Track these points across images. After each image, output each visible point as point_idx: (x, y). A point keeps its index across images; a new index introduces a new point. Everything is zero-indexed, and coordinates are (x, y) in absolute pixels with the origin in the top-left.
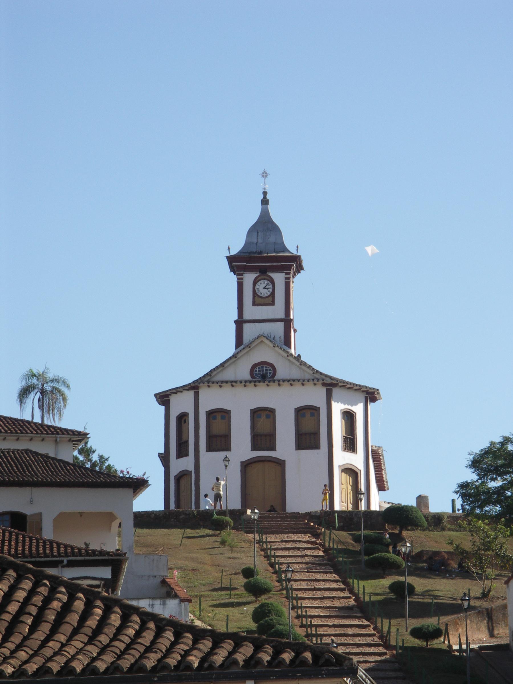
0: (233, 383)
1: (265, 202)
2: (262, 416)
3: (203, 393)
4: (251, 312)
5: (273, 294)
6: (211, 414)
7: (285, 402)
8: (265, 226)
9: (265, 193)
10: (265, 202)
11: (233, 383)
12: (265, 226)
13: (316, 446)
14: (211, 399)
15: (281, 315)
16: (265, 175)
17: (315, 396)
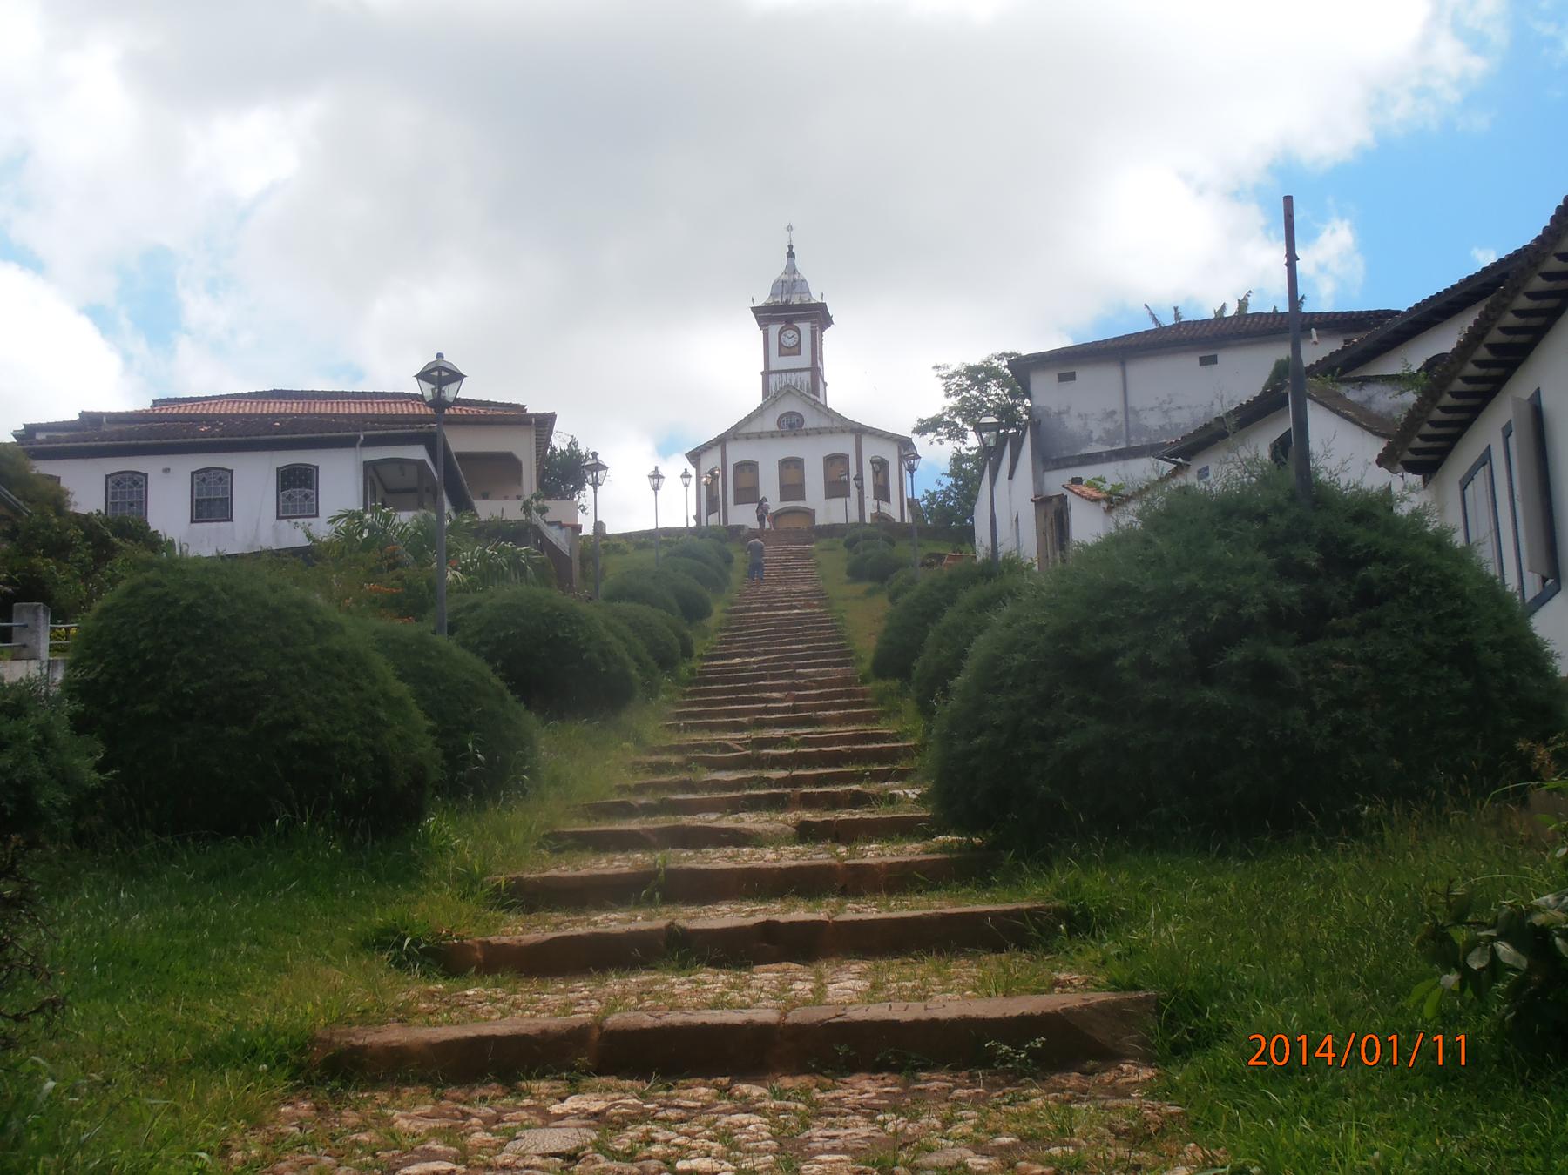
0: (760, 436)
1: (791, 255)
3: (730, 447)
4: (778, 363)
5: (799, 344)
6: (739, 467)
7: (813, 455)
8: (791, 282)
9: (791, 247)
10: (791, 255)
11: (760, 436)
12: (791, 282)
14: (738, 453)
15: (808, 364)
16: (790, 228)
17: (845, 445)
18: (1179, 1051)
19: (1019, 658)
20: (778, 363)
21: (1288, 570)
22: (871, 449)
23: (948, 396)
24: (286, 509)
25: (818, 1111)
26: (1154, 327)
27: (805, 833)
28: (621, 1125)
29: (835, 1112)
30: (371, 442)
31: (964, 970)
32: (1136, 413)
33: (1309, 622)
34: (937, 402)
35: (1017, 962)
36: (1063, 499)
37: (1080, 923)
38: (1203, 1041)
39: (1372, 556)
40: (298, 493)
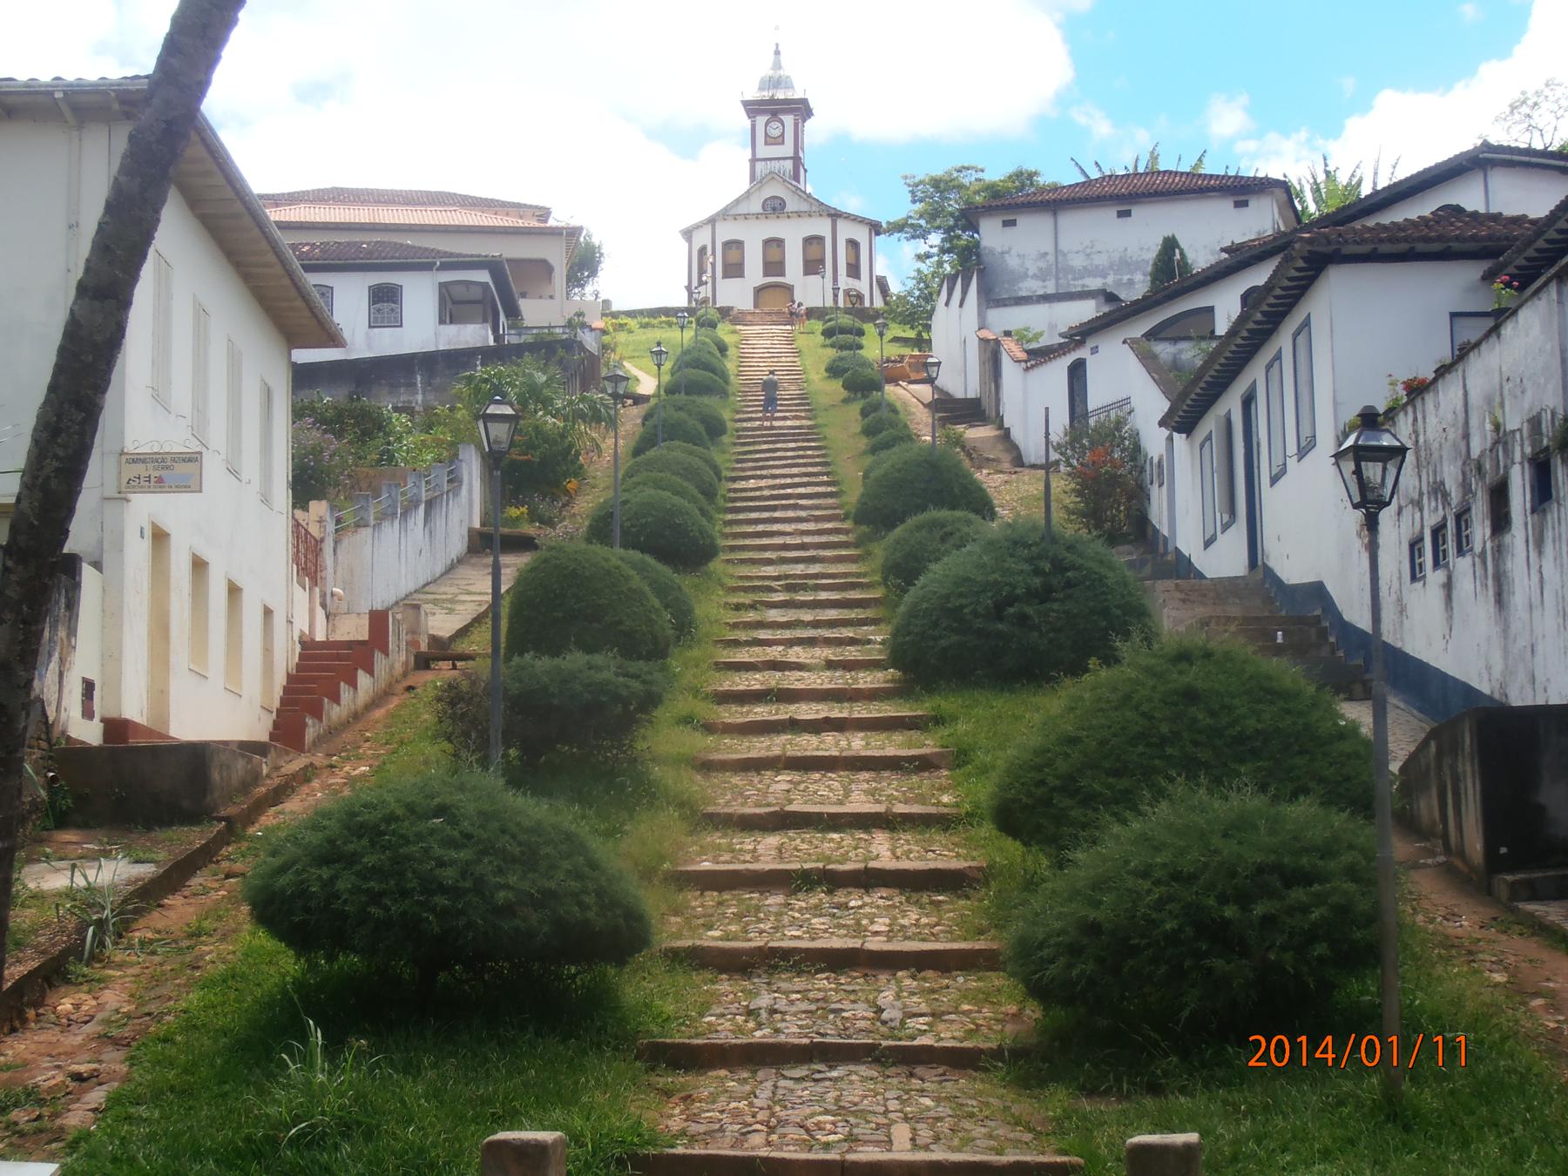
0: (746, 217)
1: (777, 53)
2: (774, 245)
4: (764, 151)
6: (728, 245)
10: (777, 53)
11: (746, 217)
14: (726, 232)
16: (777, 28)
17: (822, 227)
18: (959, 766)
19: (925, 605)
20: (764, 151)
21: (1037, 572)
22: (846, 231)
23: (914, 202)
24: (376, 320)
25: (852, 781)
26: (1082, 179)
27: (831, 665)
28: (800, 783)
29: (858, 781)
30: (445, 267)
31: (898, 737)
32: (1065, 255)
33: (1043, 595)
34: (899, 206)
35: (915, 735)
36: (997, 342)
37: (938, 720)
38: (966, 763)
39: (1073, 567)
40: (385, 306)
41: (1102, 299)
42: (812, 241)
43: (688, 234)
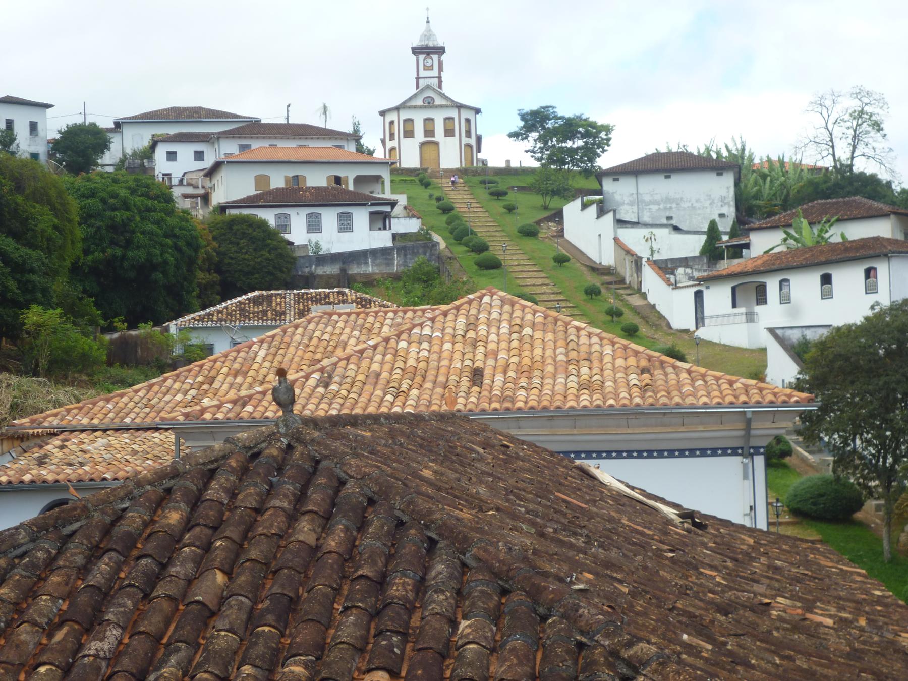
0: (415, 107)
2: (429, 121)
6: (405, 121)
13: (454, 135)
30: (372, 205)
41: (671, 229)
42: (449, 119)
43: (383, 113)
